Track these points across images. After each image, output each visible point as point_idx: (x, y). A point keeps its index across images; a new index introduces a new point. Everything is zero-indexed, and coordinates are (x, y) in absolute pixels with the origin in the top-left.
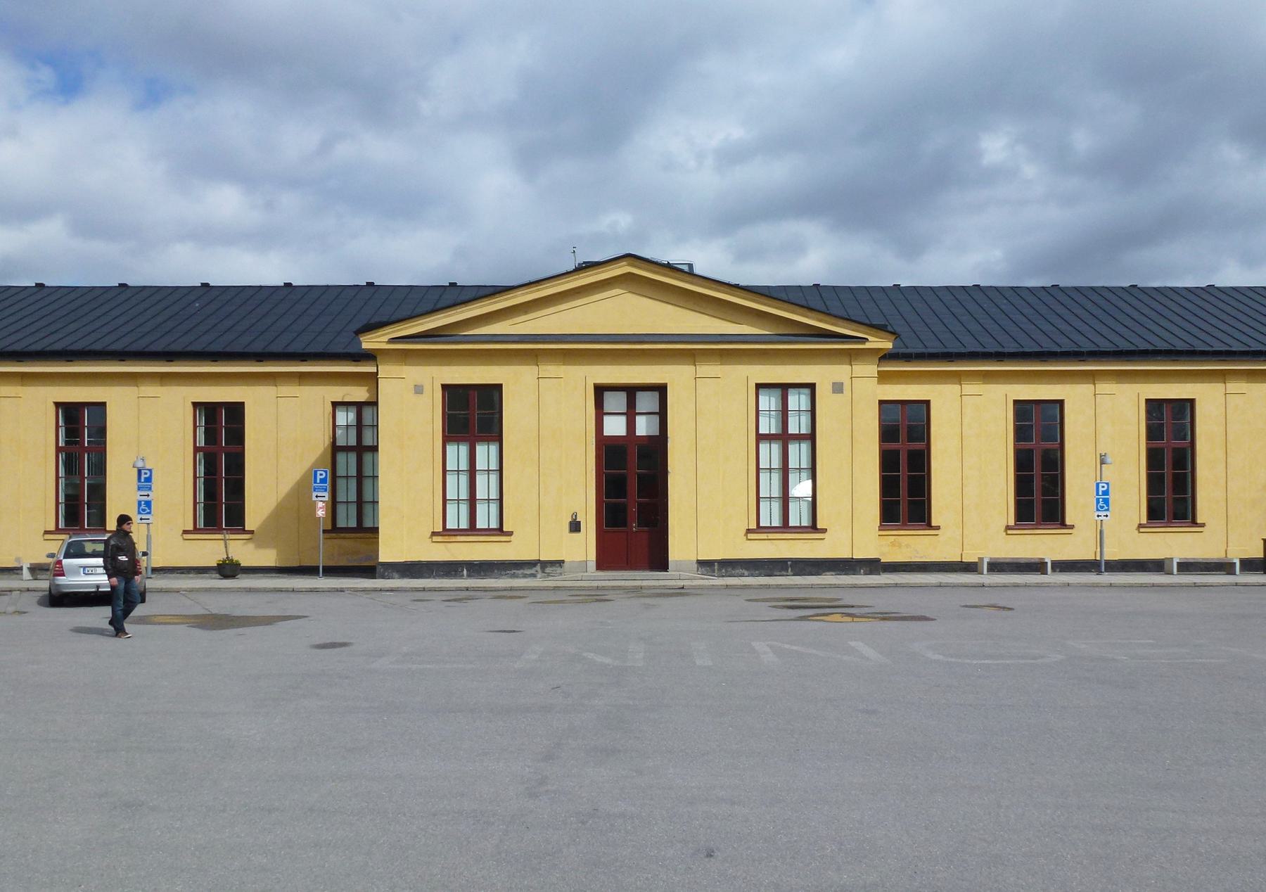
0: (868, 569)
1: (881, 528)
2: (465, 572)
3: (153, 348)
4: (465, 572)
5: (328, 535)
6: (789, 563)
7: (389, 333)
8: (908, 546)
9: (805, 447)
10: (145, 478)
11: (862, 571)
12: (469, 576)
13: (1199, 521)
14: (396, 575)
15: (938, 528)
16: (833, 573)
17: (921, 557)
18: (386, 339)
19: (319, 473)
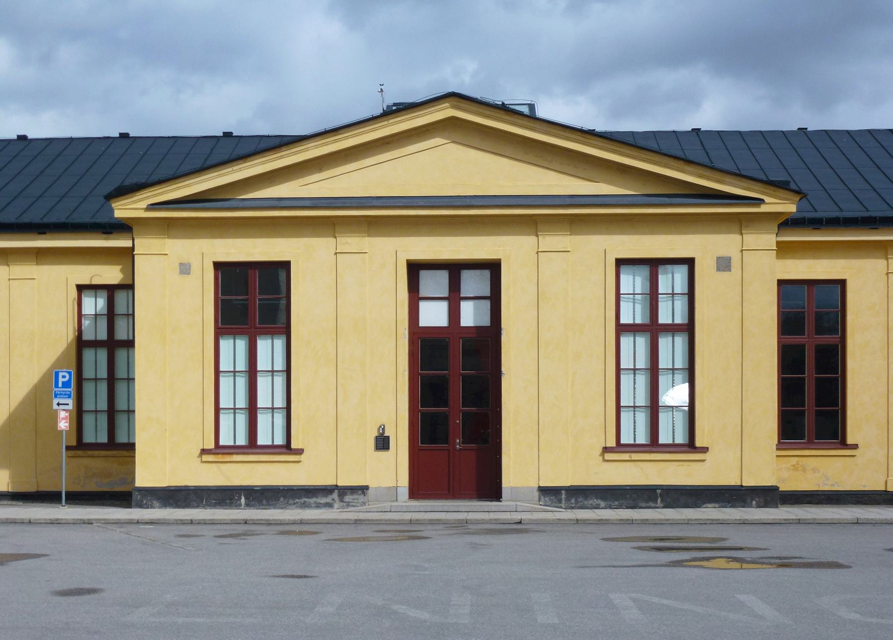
0: (762, 500)
1: (780, 446)
2: (243, 500)
3: (52, 219)
4: (243, 500)
5: (71, 453)
6: (659, 491)
7: (148, 198)
8: (814, 470)
9: (680, 341)
10: (63, 383)
11: (754, 503)
12: (248, 505)
13: (850, 441)
14: (156, 504)
15: (855, 447)
16: (717, 505)
17: (833, 485)
18: (144, 204)
19: (61, 374)
